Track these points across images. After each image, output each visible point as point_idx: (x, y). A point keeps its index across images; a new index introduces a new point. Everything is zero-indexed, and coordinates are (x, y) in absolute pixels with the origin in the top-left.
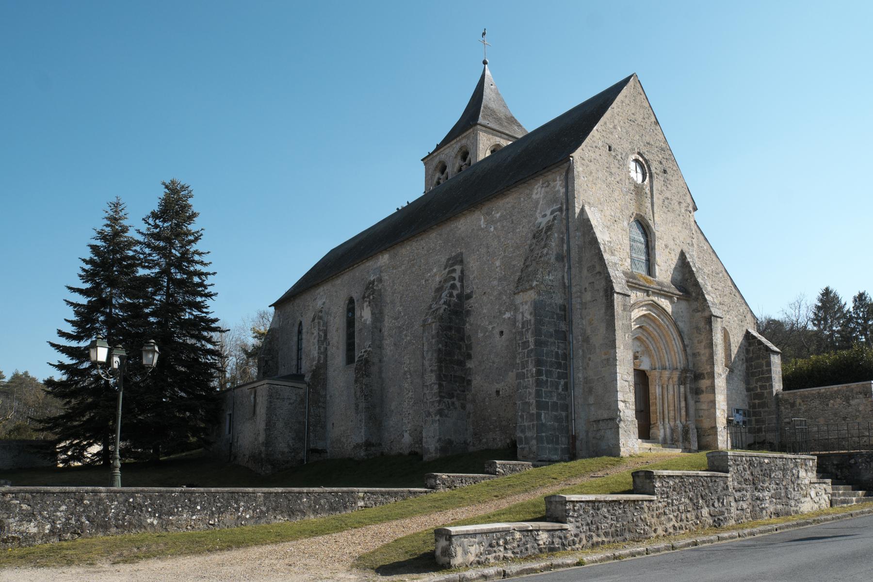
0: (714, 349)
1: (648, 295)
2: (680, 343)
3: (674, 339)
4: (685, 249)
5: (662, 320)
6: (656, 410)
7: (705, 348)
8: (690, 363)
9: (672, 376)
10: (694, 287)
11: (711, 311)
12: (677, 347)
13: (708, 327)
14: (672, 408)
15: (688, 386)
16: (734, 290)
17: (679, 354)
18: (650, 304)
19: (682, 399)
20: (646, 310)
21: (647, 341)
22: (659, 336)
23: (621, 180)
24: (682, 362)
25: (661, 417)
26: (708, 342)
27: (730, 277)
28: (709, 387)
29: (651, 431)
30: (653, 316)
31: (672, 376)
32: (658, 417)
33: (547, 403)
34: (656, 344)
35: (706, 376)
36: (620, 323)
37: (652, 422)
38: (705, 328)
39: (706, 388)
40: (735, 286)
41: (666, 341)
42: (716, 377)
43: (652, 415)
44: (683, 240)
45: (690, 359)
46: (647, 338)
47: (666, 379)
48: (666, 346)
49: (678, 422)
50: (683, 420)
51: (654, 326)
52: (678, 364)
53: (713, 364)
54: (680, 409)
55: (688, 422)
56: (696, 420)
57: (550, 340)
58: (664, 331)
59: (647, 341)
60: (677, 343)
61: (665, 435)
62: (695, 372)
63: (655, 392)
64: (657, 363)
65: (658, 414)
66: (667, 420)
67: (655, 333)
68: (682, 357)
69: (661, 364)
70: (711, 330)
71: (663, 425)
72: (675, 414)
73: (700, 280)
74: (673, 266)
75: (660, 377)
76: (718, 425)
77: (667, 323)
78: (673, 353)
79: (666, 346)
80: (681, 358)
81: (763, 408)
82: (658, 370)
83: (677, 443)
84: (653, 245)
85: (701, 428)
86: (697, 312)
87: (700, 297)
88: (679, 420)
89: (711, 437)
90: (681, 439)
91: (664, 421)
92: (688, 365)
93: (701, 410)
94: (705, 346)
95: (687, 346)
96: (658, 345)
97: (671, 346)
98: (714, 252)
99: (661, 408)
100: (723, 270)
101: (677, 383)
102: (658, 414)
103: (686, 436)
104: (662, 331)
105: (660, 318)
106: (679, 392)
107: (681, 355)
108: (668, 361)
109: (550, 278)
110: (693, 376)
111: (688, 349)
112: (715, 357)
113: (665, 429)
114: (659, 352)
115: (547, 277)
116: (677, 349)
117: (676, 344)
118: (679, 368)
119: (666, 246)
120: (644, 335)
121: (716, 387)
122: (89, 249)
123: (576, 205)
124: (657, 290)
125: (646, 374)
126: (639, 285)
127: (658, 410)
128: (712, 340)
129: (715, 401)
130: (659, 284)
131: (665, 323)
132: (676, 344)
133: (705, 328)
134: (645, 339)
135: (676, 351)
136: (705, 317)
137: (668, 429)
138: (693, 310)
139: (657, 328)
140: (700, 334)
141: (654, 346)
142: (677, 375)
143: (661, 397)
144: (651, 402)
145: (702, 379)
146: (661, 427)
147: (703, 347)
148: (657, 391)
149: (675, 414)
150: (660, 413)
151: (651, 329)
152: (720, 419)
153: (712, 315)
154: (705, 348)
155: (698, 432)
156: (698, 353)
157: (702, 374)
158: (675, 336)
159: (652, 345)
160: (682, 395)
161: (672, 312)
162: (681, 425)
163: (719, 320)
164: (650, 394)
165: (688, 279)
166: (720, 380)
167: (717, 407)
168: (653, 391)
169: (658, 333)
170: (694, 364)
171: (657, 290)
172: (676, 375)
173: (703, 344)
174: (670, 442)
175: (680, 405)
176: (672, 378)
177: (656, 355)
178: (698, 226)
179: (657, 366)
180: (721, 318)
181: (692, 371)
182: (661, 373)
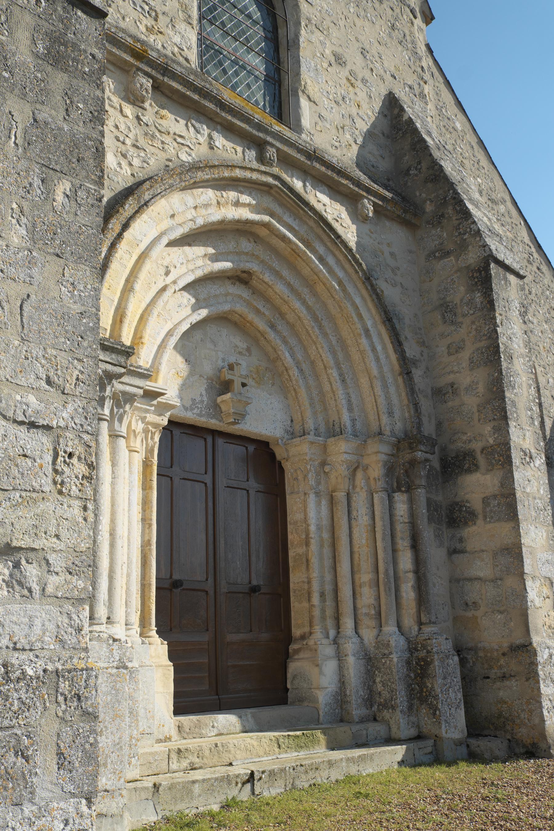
0: (504, 365)
1: (261, 159)
2: (390, 346)
3: (367, 331)
4: (402, 94)
5: (321, 259)
6: (309, 582)
7: (473, 365)
8: (425, 420)
9: (366, 461)
10: (430, 185)
11: (485, 246)
12: (377, 359)
13: (478, 297)
14: (365, 577)
15: (421, 494)
16: (536, 255)
17: (385, 386)
19: (403, 544)
20: (256, 209)
21: (271, 335)
22: (316, 319)
24: (397, 414)
25: (329, 612)
26: (484, 344)
27: (525, 221)
28: (495, 496)
29: (293, 667)
30: (284, 238)
31: (366, 461)
32: (317, 613)
34: (305, 349)
35: (481, 460)
37: (296, 632)
38: (470, 302)
39: (485, 501)
40: (539, 247)
41: (341, 341)
42: (516, 460)
43: (295, 604)
44: (392, 69)
45: (425, 405)
46: (272, 326)
47: (343, 470)
48: (340, 356)
49: (390, 628)
50: (409, 621)
51: (296, 283)
52: (385, 419)
53: (505, 418)
54: (397, 578)
55: (427, 629)
56: (456, 619)
58: (330, 302)
59: (271, 335)
60: (379, 348)
61: (342, 682)
62: (443, 449)
63: (306, 519)
64: (308, 413)
65: (316, 600)
66: (348, 623)
67: (297, 305)
69: (327, 423)
70: (490, 305)
71: (335, 642)
72: (378, 598)
73: (448, 167)
74: (363, 126)
75: (323, 464)
76: (536, 640)
77: (341, 274)
78: (364, 381)
79: (340, 356)
80: (395, 401)
81: (157, 632)
82: (311, 437)
83: (386, 714)
84: (291, 36)
85: (474, 650)
86: (441, 258)
87: (450, 210)
88: (393, 621)
89: (513, 683)
90: (401, 698)
91: (338, 627)
92: (420, 424)
93: (470, 580)
94: (471, 361)
95: (415, 363)
96: (312, 351)
97: (356, 357)
98: (481, 143)
99: (328, 577)
100: (508, 198)
101: (381, 484)
102: (316, 600)
103: (422, 685)
104: (324, 305)
105: (314, 251)
106: (392, 516)
107: (392, 390)
108: (350, 410)
110: (436, 464)
111: (417, 373)
112: (507, 394)
113: (340, 657)
114: (317, 376)
116: (380, 367)
117: (374, 349)
118: (387, 430)
119: (339, 60)
120: (258, 312)
121: (518, 495)
125: (272, 455)
127: (316, 586)
128: (493, 336)
129: (518, 546)
131: (330, 271)
132: (374, 349)
133: (470, 302)
134: (261, 325)
135: (375, 372)
136: (468, 267)
137: (351, 660)
138: (431, 255)
139: (305, 292)
140: (453, 323)
141: (299, 356)
142: (383, 457)
143: (326, 535)
144: (291, 554)
145: (469, 471)
146: (329, 650)
147: (465, 364)
148: (312, 514)
149: (378, 598)
150: (322, 595)
151: (280, 288)
152: (543, 612)
153: (491, 258)
154: (473, 365)
155: (463, 662)
156: (452, 385)
157: (469, 455)
158: (369, 324)
159: (291, 350)
160: (401, 529)
161: (357, 243)
162: (402, 641)
164: (290, 528)
165: (408, 170)
166: (529, 473)
167: (527, 568)
168: (299, 516)
169: (308, 308)
170: (439, 425)
173: (465, 355)
175: (395, 563)
176: (366, 468)
177: (308, 388)
178: (435, 61)
179: (310, 424)
180: (521, 277)
181: (432, 443)
182: (325, 448)
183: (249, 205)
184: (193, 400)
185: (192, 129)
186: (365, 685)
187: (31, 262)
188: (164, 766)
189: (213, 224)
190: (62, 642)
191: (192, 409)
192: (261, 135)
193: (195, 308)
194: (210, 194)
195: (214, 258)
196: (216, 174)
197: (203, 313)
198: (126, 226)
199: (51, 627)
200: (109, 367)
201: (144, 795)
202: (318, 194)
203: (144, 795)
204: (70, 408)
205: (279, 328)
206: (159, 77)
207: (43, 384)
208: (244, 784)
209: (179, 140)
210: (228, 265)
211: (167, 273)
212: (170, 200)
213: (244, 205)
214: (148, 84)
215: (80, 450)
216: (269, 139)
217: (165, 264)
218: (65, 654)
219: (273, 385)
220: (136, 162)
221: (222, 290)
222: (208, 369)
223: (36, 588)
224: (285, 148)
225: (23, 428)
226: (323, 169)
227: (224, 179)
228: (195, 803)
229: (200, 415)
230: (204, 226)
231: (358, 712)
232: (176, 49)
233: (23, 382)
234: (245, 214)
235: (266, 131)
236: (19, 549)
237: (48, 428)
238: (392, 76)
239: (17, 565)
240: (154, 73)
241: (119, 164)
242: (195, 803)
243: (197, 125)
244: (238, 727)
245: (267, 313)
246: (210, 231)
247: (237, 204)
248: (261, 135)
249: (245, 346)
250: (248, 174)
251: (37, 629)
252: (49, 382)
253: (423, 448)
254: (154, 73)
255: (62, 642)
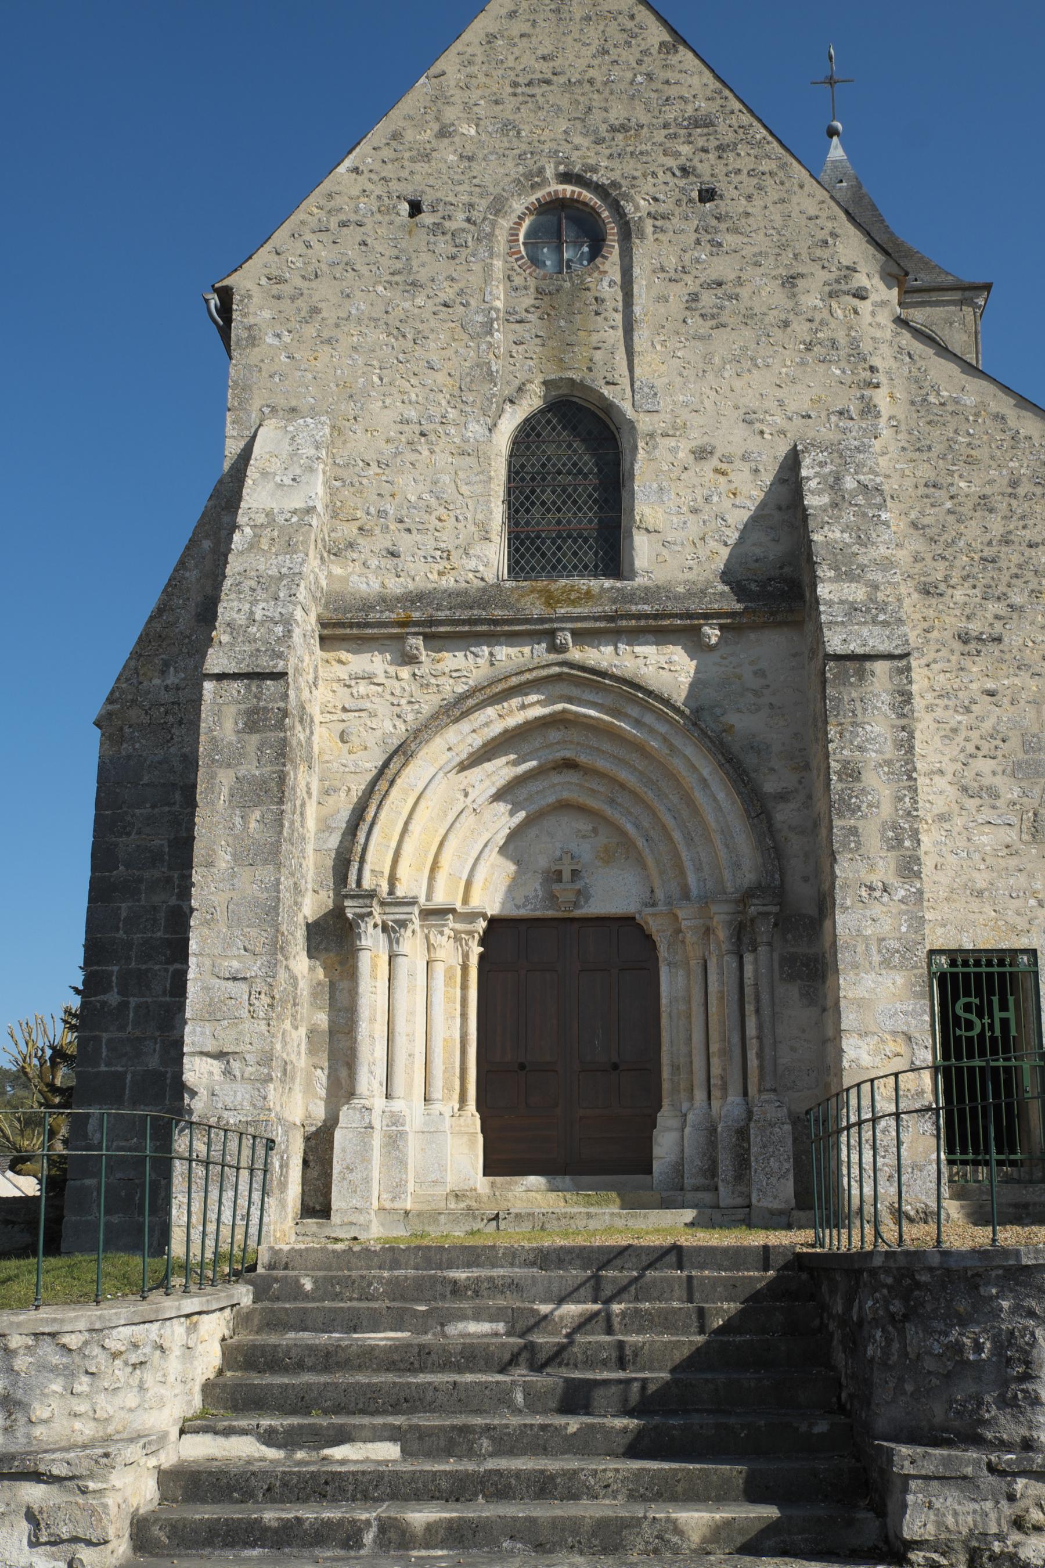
1: (553, 648)
18: (559, 677)
23: (461, 293)
33: (121, 1077)
36: (225, 779)
46: (612, 802)
57: (147, 875)
68: (744, 842)
108: (699, 869)
109: (169, 682)
115: (157, 681)
118: (729, 887)
122: (502, 807)
123: (230, 430)
124: (596, 619)
126: (495, 622)
130: (649, 594)
158: (706, 772)
163: (881, 667)
171: (596, 619)
172: (720, 916)
174: (701, 1181)
183: (538, 702)
184: (526, 898)
185: (470, 656)
186: (705, 1155)
187: (234, 875)
188: (443, 1205)
189: (494, 739)
190: (254, 1105)
191: (524, 906)
192: (546, 626)
193: (512, 813)
194: (490, 711)
195: (515, 763)
196: (480, 697)
197: (522, 815)
198: (392, 783)
199: (247, 1096)
200: (358, 910)
201: (396, 1218)
202: (638, 649)
203: (396, 1218)
204: (259, 963)
205: (619, 800)
206: (428, 630)
207: (242, 952)
208: (490, 1220)
209: (455, 674)
210: (533, 763)
211: (466, 795)
212: (447, 736)
213: (533, 704)
214: (419, 642)
215: (266, 988)
216: (555, 625)
217: (462, 787)
218: (256, 1112)
219: (627, 858)
220: (410, 717)
221: (546, 784)
222: (543, 862)
223: (238, 1074)
224: (579, 625)
225: (230, 983)
226: (633, 622)
227: (496, 694)
228: (442, 1228)
229: (534, 910)
230: (484, 745)
231: (693, 1181)
232: (471, 575)
233: (229, 953)
234: (538, 711)
235: (551, 620)
236: (228, 1053)
237: (245, 979)
238: (803, 417)
239: (228, 1062)
240: (421, 630)
241: (395, 726)
242: (442, 1228)
243: (473, 649)
244: (543, 1187)
245: (602, 790)
246: (513, 737)
247: (523, 707)
248: (546, 626)
249: (590, 828)
250: (544, 673)
251: (239, 1098)
252: (246, 950)
253: (756, 901)
254: (421, 630)
255: (254, 1105)
